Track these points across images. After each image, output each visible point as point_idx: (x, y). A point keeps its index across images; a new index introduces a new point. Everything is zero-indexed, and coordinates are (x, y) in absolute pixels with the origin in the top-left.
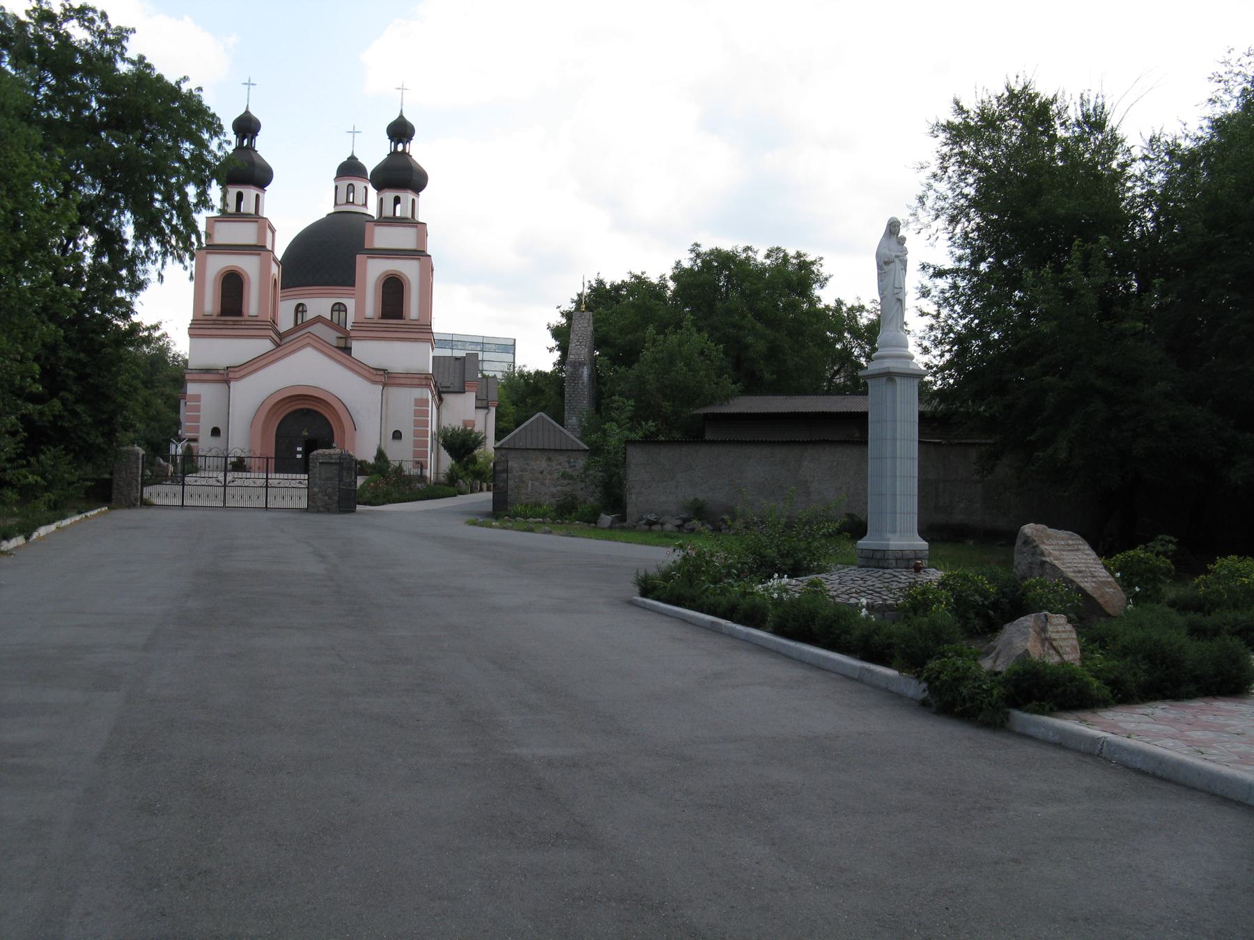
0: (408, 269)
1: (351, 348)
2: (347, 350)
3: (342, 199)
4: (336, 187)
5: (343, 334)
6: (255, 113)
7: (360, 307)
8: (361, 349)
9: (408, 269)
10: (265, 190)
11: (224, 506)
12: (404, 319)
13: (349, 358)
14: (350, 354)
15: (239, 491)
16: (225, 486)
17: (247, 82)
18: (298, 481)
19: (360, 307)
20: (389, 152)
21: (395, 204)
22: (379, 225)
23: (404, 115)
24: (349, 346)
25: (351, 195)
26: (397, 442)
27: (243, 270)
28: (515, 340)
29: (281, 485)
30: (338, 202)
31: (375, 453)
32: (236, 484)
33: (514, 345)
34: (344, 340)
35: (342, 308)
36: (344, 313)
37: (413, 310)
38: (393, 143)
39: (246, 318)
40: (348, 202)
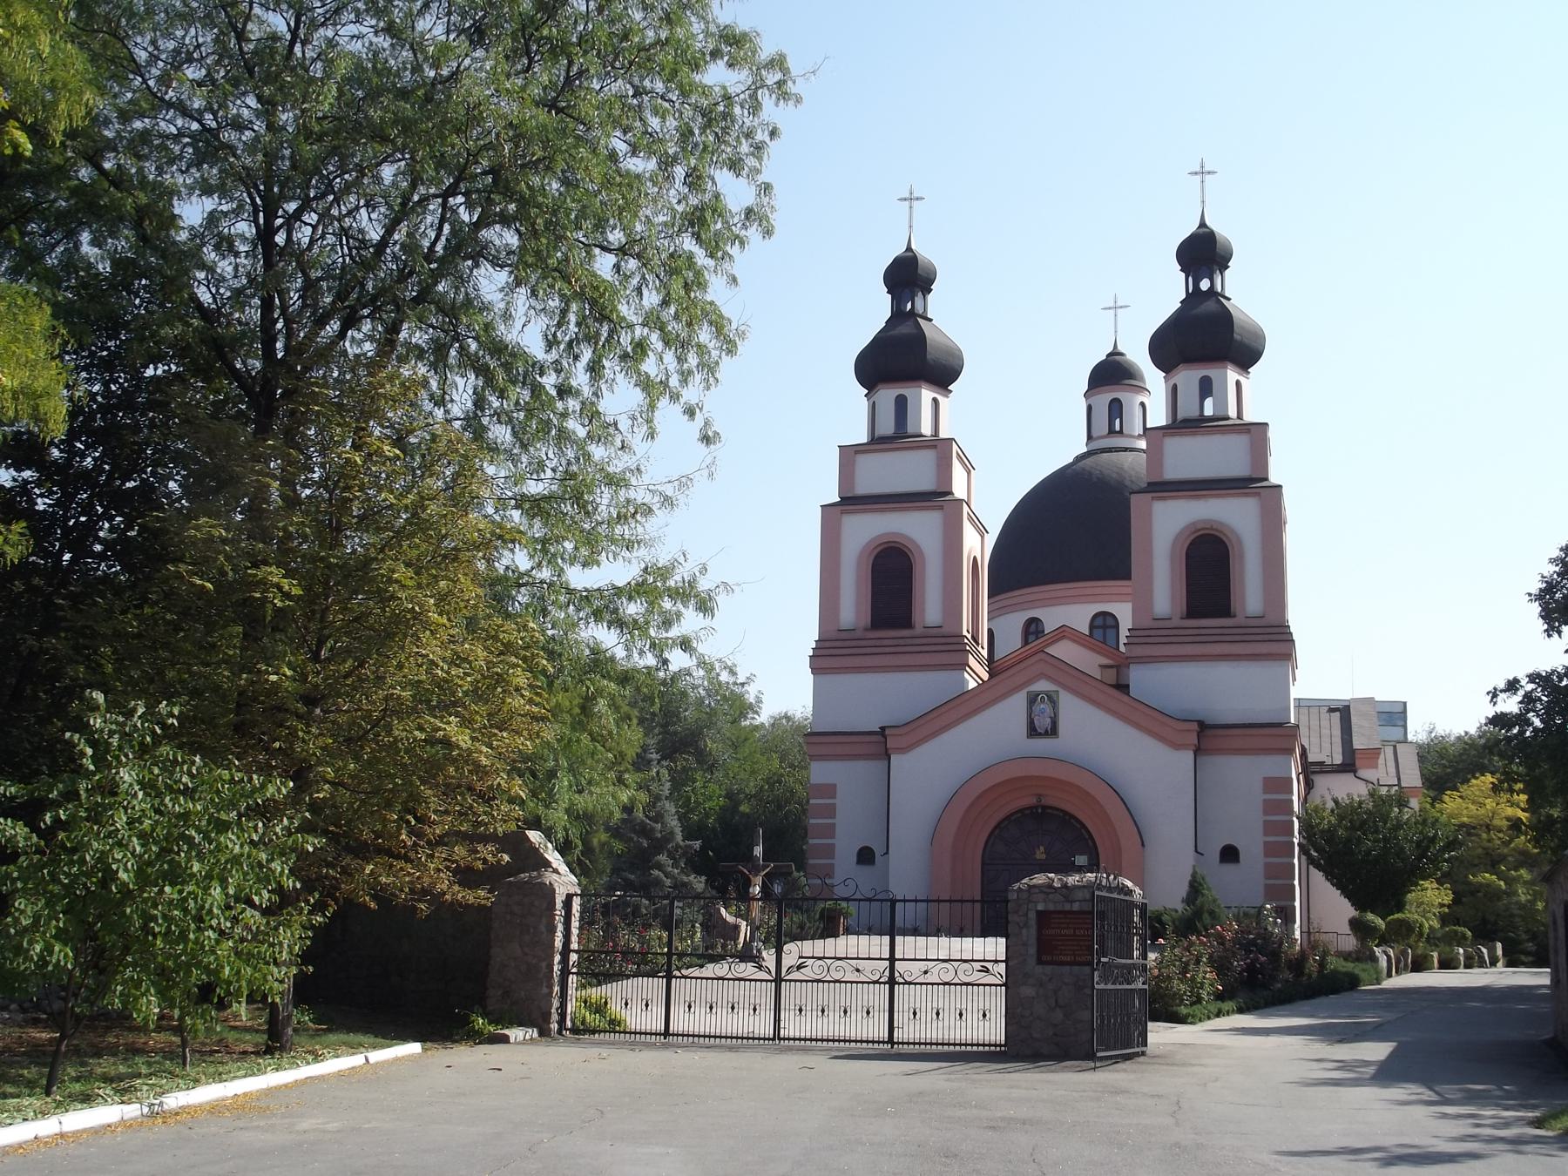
0: (1234, 514)
1: (1128, 686)
2: (1123, 687)
3: (1101, 426)
4: (1089, 409)
5: (1112, 659)
6: (923, 250)
7: (1142, 603)
8: (1148, 680)
9: (1234, 514)
10: (951, 391)
11: (776, 1036)
12: (1235, 616)
13: (1125, 698)
14: (1128, 694)
15: (821, 993)
16: (778, 980)
17: (907, 195)
18: (977, 966)
19: (1142, 603)
20: (1183, 296)
21: (1203, 396)
22: (1173, 435)
23: (1208, 223)
24: (1122, 682)
25: (1118, 421)
26: (1230, 868)
27: (914, 542)
28: (1405, 704)
29: (930, 978)
30: (1095, 434)
31: (1183, 889)
32: (807, 973)
33: (1404, 712)
34: (1114, 670)
35: (1110, 621)
36: (1114, 630)
37: (1250, 598)
38: (1190, 279)
39: (918, 630)
40: (1112, 431)
